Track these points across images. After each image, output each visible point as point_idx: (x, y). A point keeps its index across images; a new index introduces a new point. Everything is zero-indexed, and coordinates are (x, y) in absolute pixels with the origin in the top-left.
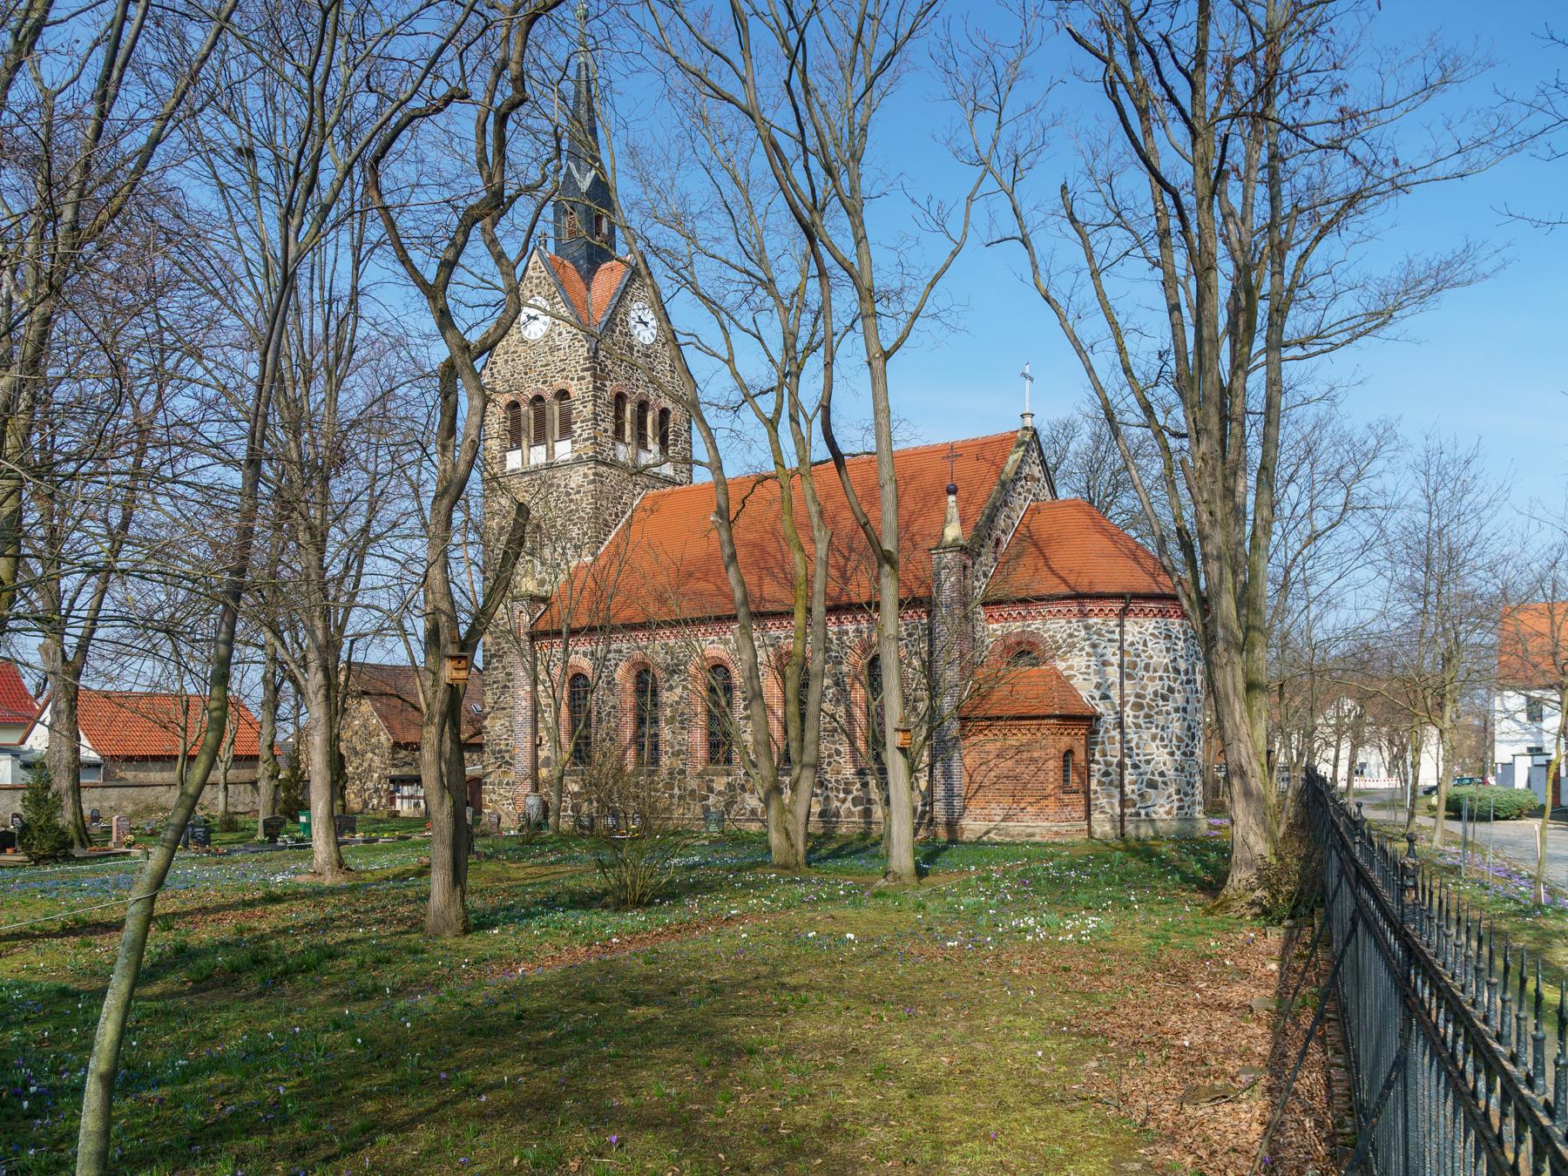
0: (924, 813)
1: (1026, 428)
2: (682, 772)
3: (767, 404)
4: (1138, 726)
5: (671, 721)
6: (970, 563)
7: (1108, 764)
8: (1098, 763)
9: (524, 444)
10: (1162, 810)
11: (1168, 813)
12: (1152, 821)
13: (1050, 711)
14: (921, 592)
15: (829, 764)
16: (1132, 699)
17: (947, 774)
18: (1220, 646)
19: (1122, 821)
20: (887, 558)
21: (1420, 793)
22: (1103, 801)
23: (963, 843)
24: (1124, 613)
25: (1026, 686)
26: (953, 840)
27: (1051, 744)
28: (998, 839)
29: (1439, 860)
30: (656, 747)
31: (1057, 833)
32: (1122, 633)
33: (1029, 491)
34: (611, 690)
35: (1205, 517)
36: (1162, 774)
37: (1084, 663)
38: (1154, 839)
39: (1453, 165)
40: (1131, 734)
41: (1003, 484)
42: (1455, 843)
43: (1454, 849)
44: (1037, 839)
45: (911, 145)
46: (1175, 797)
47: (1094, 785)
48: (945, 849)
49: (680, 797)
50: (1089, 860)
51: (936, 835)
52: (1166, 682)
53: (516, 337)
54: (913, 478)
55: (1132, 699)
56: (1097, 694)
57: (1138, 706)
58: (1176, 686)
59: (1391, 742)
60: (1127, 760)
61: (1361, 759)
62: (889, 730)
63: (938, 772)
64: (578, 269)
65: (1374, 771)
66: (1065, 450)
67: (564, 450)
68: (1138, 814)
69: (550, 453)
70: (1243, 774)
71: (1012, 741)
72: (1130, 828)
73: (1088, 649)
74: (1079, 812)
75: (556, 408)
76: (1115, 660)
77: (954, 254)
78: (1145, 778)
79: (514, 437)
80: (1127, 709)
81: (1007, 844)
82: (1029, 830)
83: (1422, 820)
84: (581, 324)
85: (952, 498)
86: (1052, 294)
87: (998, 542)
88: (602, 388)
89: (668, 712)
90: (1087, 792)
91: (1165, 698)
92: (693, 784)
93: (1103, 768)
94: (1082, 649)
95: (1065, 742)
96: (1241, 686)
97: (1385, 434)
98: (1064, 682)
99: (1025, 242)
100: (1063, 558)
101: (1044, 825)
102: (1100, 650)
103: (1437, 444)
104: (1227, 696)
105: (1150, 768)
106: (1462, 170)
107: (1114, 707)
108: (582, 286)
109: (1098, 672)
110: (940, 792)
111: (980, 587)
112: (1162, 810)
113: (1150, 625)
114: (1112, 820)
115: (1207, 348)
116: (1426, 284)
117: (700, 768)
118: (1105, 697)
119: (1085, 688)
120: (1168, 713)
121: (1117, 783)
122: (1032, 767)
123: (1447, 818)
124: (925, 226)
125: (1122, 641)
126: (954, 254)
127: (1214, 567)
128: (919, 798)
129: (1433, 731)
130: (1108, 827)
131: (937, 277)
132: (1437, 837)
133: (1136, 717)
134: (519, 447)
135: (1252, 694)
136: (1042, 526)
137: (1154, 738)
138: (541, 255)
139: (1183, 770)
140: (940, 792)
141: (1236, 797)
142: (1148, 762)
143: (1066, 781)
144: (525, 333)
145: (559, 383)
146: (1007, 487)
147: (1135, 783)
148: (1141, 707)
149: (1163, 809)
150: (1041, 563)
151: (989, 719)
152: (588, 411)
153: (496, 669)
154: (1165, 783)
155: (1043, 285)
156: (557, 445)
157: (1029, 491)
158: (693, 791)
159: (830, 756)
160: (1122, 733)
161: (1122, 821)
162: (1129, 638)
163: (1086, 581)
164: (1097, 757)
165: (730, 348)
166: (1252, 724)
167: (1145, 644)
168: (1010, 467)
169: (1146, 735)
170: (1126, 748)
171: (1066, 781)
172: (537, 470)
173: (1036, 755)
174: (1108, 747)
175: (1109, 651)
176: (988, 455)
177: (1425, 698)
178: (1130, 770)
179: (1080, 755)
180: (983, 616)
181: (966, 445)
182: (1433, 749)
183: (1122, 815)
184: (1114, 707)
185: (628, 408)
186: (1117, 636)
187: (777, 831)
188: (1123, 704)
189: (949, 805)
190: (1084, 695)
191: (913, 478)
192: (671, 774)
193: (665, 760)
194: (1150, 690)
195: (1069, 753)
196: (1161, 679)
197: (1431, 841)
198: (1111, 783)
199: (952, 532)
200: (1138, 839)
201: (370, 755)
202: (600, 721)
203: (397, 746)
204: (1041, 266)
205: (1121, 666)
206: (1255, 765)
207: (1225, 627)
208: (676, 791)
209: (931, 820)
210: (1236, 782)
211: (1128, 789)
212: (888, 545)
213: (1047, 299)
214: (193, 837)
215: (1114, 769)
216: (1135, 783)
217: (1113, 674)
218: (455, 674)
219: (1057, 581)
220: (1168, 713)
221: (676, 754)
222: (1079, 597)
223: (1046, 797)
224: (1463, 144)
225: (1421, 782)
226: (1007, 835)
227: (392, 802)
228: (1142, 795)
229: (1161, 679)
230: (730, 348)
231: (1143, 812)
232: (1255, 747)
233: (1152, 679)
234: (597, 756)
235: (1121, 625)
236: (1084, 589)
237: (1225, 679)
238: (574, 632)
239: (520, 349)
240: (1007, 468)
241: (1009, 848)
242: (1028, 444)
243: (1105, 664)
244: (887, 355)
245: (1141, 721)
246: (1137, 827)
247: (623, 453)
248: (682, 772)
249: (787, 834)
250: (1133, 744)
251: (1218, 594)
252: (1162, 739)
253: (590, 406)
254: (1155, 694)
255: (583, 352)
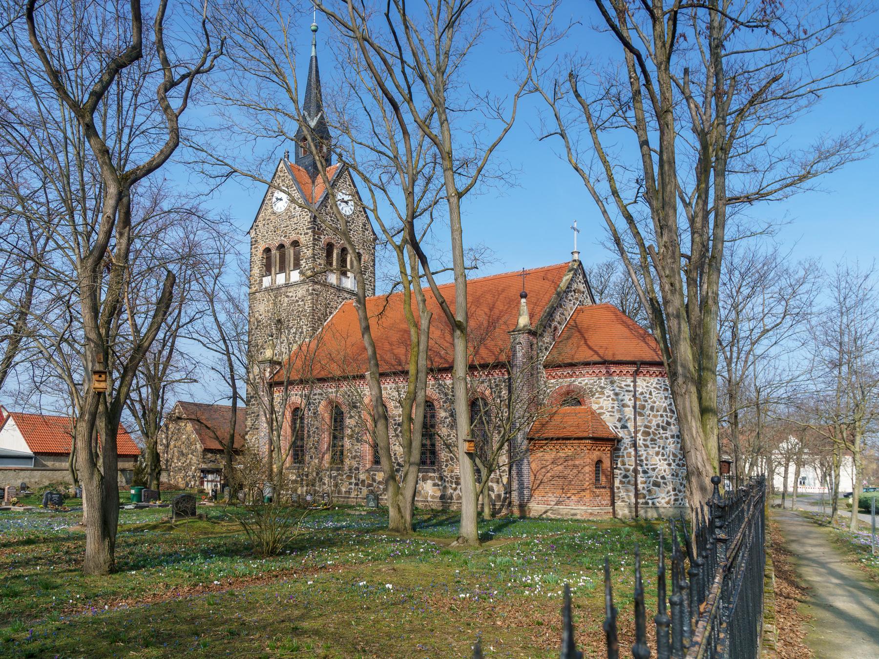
0: (505, 498)
1: (575, 261)
2: (357, 469)
3: (398, 240)
4: (646, 446)
5: (351, 437)
6: (535, 341)
7: (627, 470)
8: (620, 469)
9: (273, 272)
10: (663, 501)
11: (668, 503)
12: (657, 508)
13: (585, 435)
14: (503, 358)
15: (446, 466)
16: (642, 429)
17: (520, 474)
18: (680, 380)
19: (636, 507)
20: (458, 326)
21: (841, 496)
22: (623, 494)
23: (530, 518)
24: (636, 373)
25: (569, 419)
26: (523, 517)
27: (587, 456)
28: (553, 516)
29: (855, 541)
30: (342, 453)
31: (591, 514)
32: (635, 386)
33: (577, 299)
34: (315, 417)
35: (667, 287)
36: (663, 478)
37: (610, 405)
38: (657, 519)
39: (850, 74)
40: (642, 452)
41: (558, 294)
42: (866, 529)
43: (865, 533)
44: (578, 517)
45: (484, 73)
46: (672, 493)
47: (617, 483)
48: (514, 522)
49: (356, 484)
50: (607, 533)
51: (512, 513)
52: (665, 419)
53: (270, 211)
54: (503, 291)
55: (642, 429)
56: (619, 425)
57: (646, 434)
58: (672, 421)
59: (822, 465)
60: (639, 468)
61: (802, 475)
62: (460, 441)
63: (514, 473)
64: (308, 172)
65: (812, 482)
66: (608, 280)
67: (295, 276)
68: (647, 503)
69: (288, 278)
70: (699, 474)
71: (561, 454)
72: (641, 512)
73: (612, 396)
74: (607, 501)
75: (292, 251)
76: (631, 403)
77: (506, 131)
78: (652, 480)
79: (268, 268)
80: (639, 435)
81: (557, 520)
82: (573, 512)
83: (842, 512)
84: (307, 205)
85: (523, 300)
86: (580, 166)
87: (556, 329)
88: (319, 239)
89: (349, 432)
90: (612, 489)
91: (664, 429)
92: (362, 477)
93: (623, 472)
94: (609, 396)
95: (595, 455)
96: (696, 409)
97: (811, 269)
98: (596, 417)
99: (563, 135)
100: (595, 340)
101: (583, 508)
102: (620, 397)
103: (845, 269)
104: (686, 416)
105: (654, 474)
106: (856, 79)
107: (630, 434)
108: (310, 181)
109: (619, 411)
110: (515, 485)
111: (544, 356)
112: (663, 501)
113: (654, 381)
114: (629, 506)
115: (666, 167)
116: (830, 156)
117: (368, 466)
118: (624, 427)
119: (611, 422)
120: (667, 438)
121: (633, 482)
122: (575, 471)
123: (859, 512)
124: (489, 115)
125: (635, 391)
126: (506, 131)
127: (674, 323)
128: (502, 489)
129: (848, 459)
130: (626, 511)
131: (495, 146)
132: (853, 524)
133: (644, 440)
134: (270, 275)
135: (706, 417)
136: (584, 320)
137: (657, 454)
138: (285, 163)
139: (677, 476)
140: (515, 485)
141: (694, 491)
142: (654, 470)
143: (597, 479)
144: (275, 209)
145: (294, 237)
146: (561, 296)
147: (645, 482)
148: (648, 434)
149: (664, 499)
150: (583, 342)
151: (546, 439)
152: (309, 253)
153: (253, 405)
154: (665, 484)
155: (574, 161)
156: (292, 273)
157: (577, 299)
158: (363, 481)
159: (447, 461)
160: (636, 450)
161: (636, 507)
162: (640, 390)
163: (611, 353)
164: (619, 465)
165: (375, 202)
166: (706, 438)
167: (651, 394)
168: (563, 284)
169: (651, 451)
170: (639, 461)
171: (597, 479)
172: (279, 288)
173: (577, 463)
174: (626, 459)
175: (627, 398)
176: (549, 276)
177: (841, 432)
178: (641, 475)
179: (607, 463)
180: (545, 375)
181: (537, 272)
182: (849, 470)
183: (637, 503)
184: (630, 434)
185: (335, 252)
186: (632, 388)
187: (393, 507)
188: (636, 432)
189: (521, 494)
190: (610, 425)
191: (503, 291)
192: (350, 470)
193: (347, 462)
194: (654, 423)
195: (599, 462)
196: (662, 416)
197: (849, 527)
198: (629, 482)
199: (523, 321)
200: (646, 520)
201: (190, 456)
202: (309, 436)
203: (207, 451)
204: (573, 148)
205: (635, 407)
206: (708, 467)
207: (683, 366)
208: (353, 480)
209: (510, 503)
210: (694, 479)
211: (640, 486)
212: (460, 318)
213: (577, 169)
214: (51, 500)
215: (631, 474)
216: (645, 482)
217: (629, 412)
218: (97, 385)
219: (593, 353)
220: (667, 438)
221: (354, 458)
222: (604, 363)
223: (583, 490)
224: (856, 59)
225: (840, 490)
226: (559, 514)
227: (202, 483)
228: (649, 491)
229: (662, 416)
230: (375, 202)
231: (650, 502)
232: (708, 454)
233: (655, 416)
234: (307, 458)
235: (635, 382)
236: (610, 358)
237: (684, 404)
238: (291, 383)
239: (272, 218)
240: (562, 285)
241: (557, 523)
242: (576, 270)
243: (624, 406)
244: (460, 195)
245: (648, 443)
246: (646, 512)
247: (333, 279)
248: (357, 469)
249: (399, 509)
250: (643, 458)
251: (677, 342)
252: (663, 455)
253: (310, 251)
254: (658, 426)
255: (308, 218)
